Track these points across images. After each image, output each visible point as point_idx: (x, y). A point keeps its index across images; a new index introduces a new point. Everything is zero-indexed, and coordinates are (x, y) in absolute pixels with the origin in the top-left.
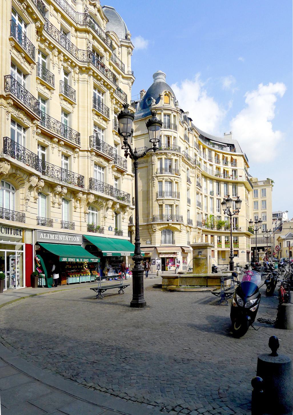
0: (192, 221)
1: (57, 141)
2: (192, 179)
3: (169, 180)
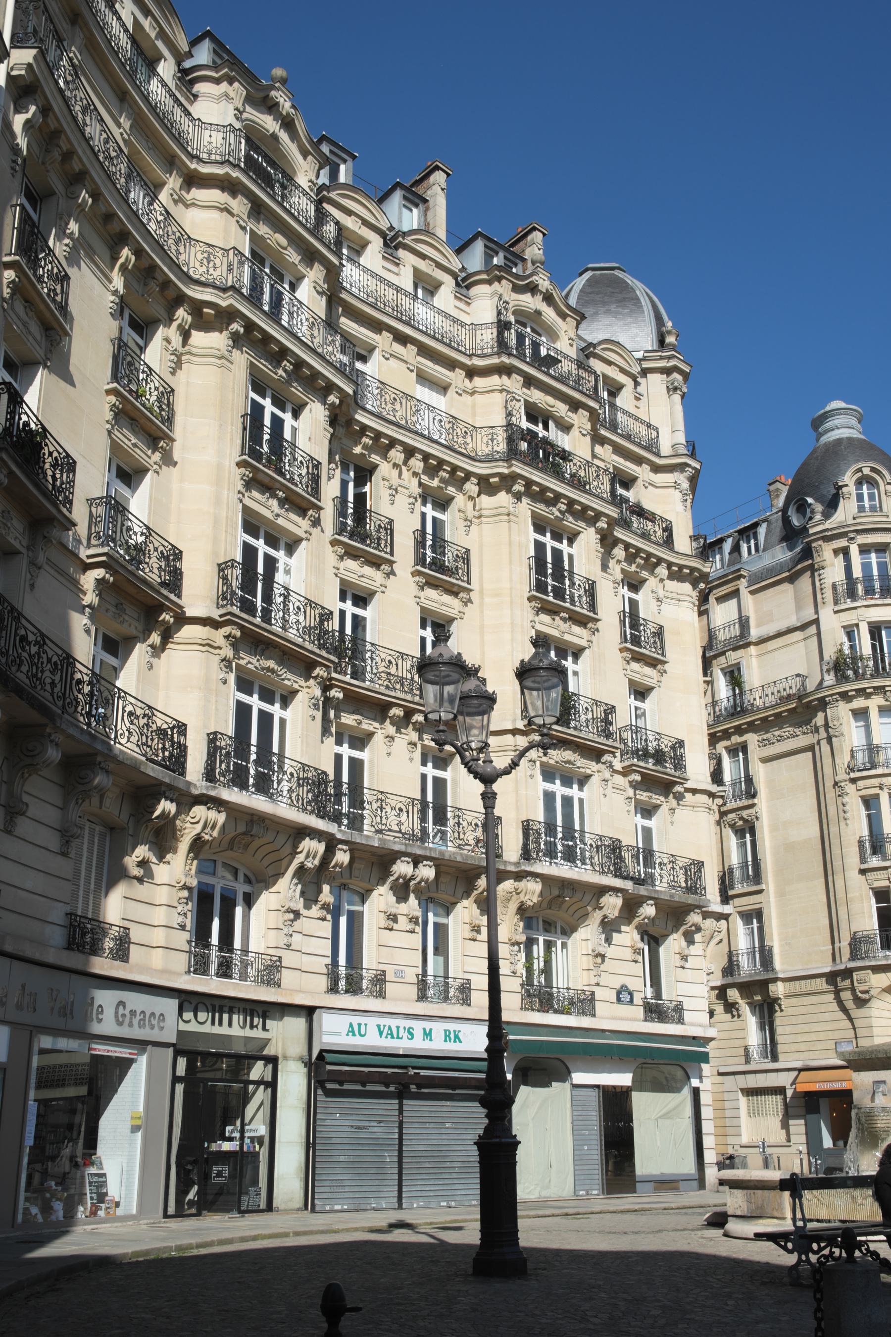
1: (402, 714)
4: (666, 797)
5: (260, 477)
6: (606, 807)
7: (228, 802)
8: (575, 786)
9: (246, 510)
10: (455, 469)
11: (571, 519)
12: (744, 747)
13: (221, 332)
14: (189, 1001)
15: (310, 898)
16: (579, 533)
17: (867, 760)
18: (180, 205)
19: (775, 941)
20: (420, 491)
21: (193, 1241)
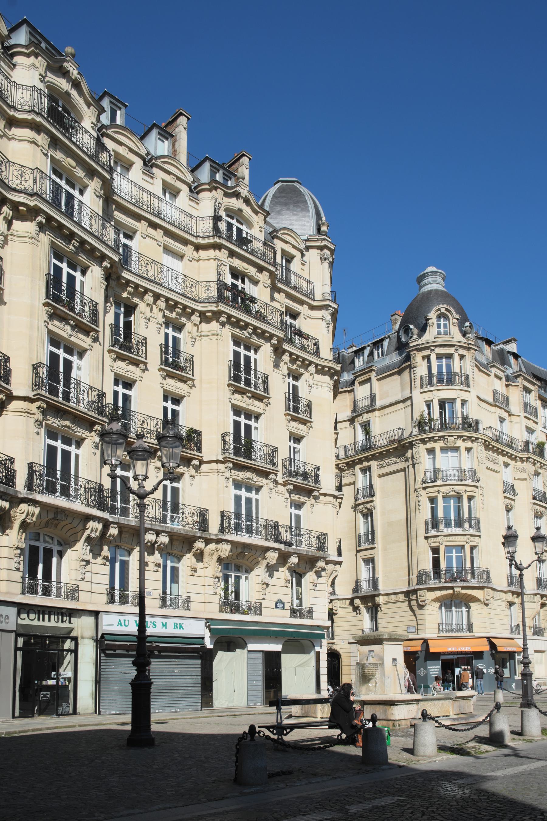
3: (453, 493)
4: (309, 498)
5: (58, 312)
6: (273, 504)
7: (41, 502)
8: (254, 492)
9: (50, 332)
10: (185, 307)
11: (255, 338)
12: (369, 468)
13: (32, 222)
14: (23, 608)
15: (96, 553)
16: (260, 346)
17: (432, 477)
18: (5, 138)
19: (380, 574)
20: (164, 320)
21: (17, 730)
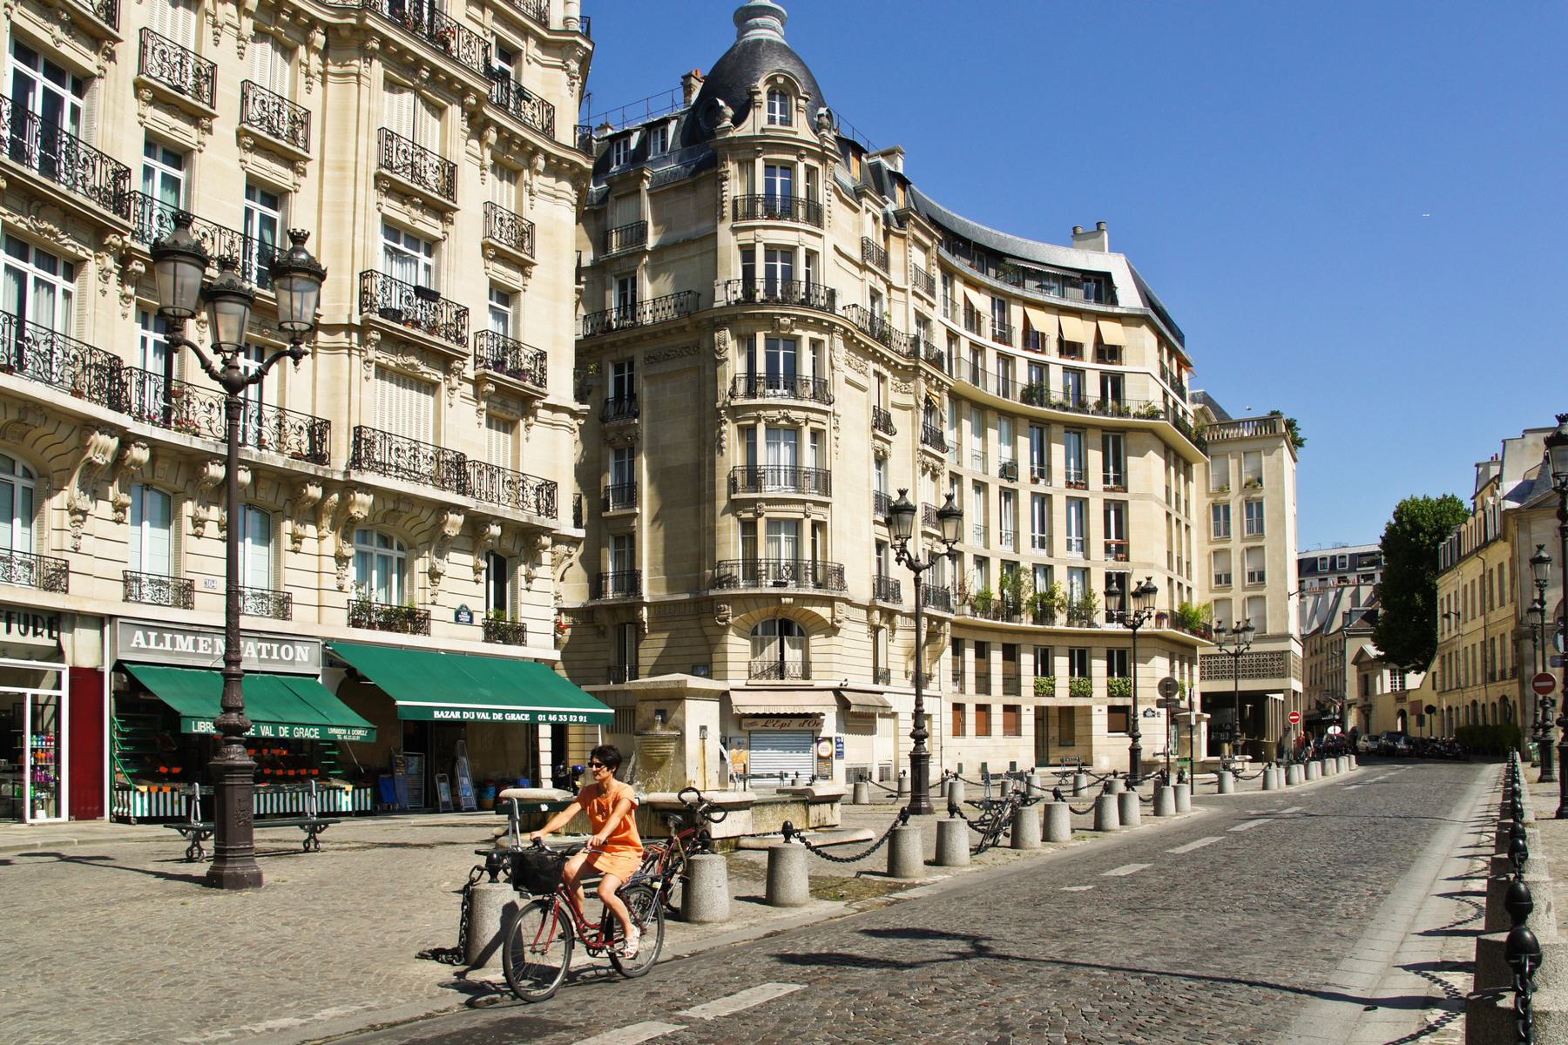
0: (898, 585)
2: (899, 419)
3: (783, 422)
